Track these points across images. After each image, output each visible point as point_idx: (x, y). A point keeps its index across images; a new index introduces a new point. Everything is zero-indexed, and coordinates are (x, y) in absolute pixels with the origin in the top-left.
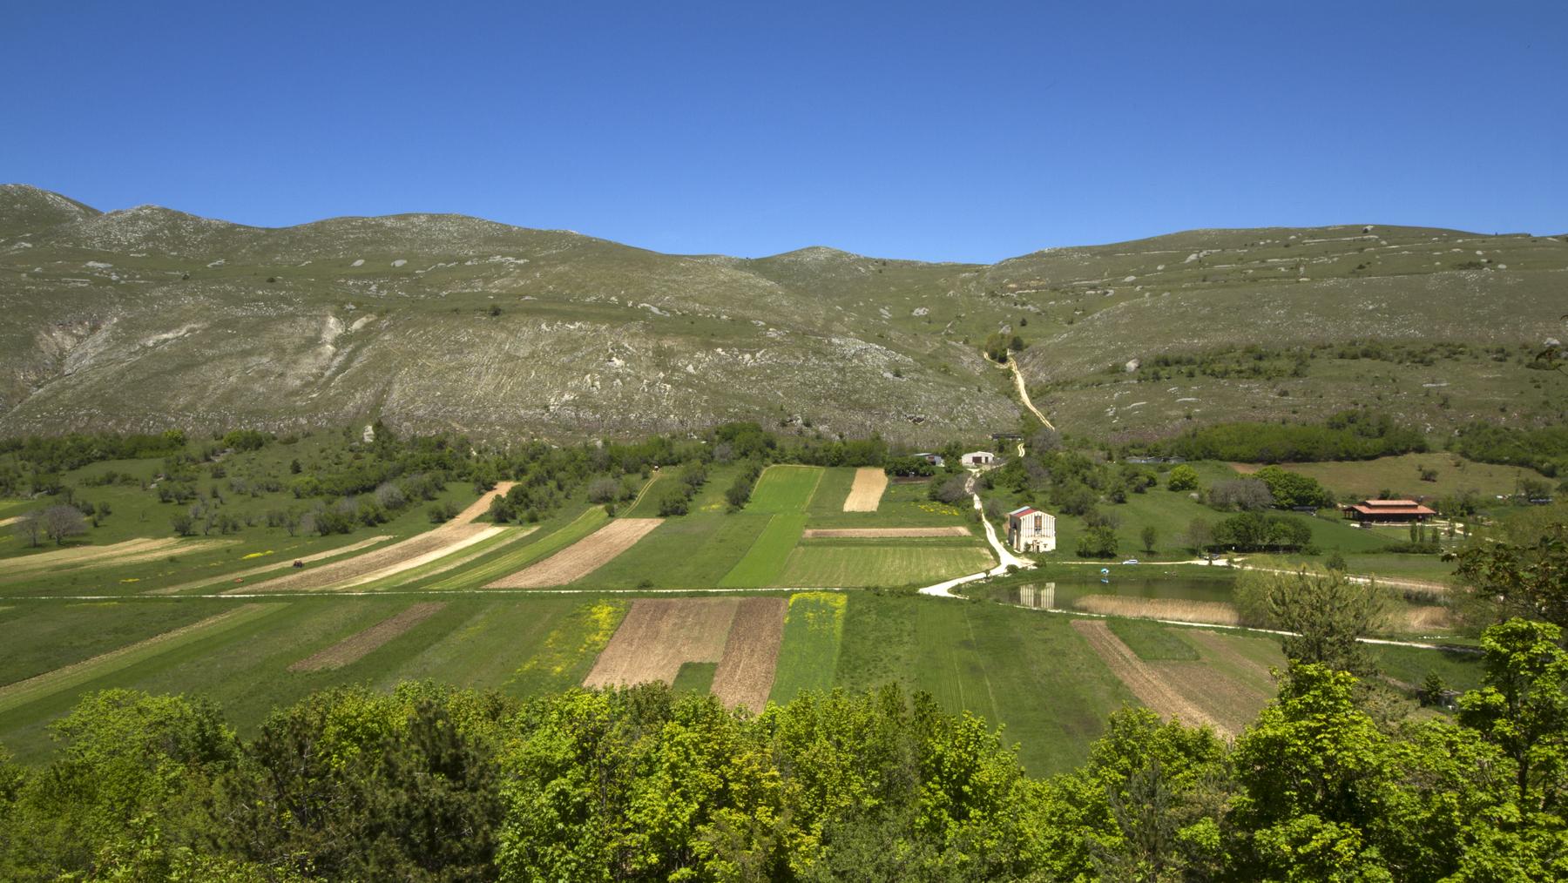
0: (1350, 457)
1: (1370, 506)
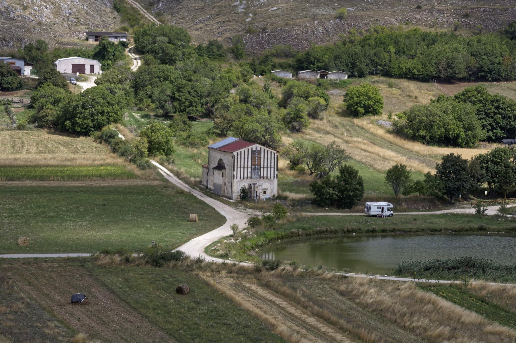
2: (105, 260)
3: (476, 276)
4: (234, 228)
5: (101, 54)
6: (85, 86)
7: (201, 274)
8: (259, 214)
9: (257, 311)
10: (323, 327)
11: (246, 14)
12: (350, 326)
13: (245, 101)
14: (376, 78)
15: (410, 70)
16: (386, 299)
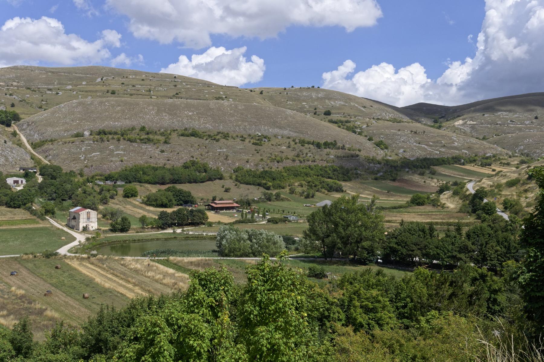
0: (195, 182)
1: (216, 204)
2: (25, 257)
3: (172, 255)
4: (80, 242)
5: (27, 175)
6: (19, 188)
7: (66, 260)
8: (90, 236)
9: (88, 274)
10: (114, 278)
11: (85, 160)
12: (124, 277)
13: (85, 193)
14: (135, 183)
15: (148, 180)
16: (138, 266)
